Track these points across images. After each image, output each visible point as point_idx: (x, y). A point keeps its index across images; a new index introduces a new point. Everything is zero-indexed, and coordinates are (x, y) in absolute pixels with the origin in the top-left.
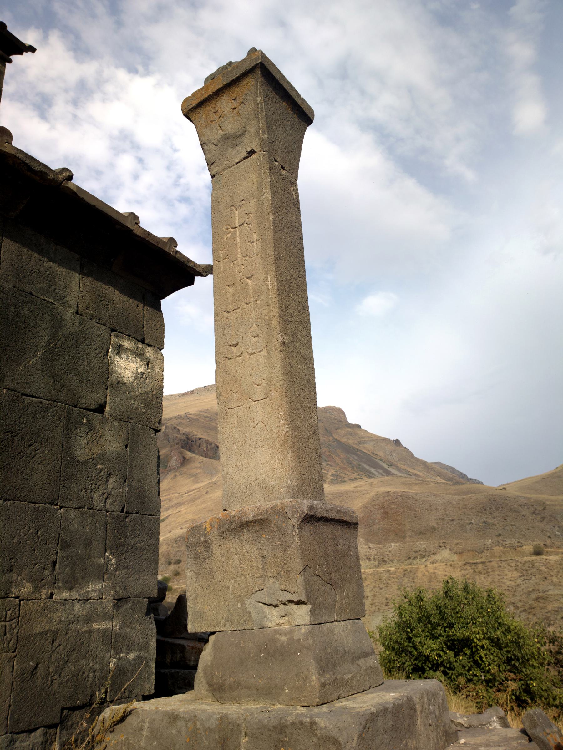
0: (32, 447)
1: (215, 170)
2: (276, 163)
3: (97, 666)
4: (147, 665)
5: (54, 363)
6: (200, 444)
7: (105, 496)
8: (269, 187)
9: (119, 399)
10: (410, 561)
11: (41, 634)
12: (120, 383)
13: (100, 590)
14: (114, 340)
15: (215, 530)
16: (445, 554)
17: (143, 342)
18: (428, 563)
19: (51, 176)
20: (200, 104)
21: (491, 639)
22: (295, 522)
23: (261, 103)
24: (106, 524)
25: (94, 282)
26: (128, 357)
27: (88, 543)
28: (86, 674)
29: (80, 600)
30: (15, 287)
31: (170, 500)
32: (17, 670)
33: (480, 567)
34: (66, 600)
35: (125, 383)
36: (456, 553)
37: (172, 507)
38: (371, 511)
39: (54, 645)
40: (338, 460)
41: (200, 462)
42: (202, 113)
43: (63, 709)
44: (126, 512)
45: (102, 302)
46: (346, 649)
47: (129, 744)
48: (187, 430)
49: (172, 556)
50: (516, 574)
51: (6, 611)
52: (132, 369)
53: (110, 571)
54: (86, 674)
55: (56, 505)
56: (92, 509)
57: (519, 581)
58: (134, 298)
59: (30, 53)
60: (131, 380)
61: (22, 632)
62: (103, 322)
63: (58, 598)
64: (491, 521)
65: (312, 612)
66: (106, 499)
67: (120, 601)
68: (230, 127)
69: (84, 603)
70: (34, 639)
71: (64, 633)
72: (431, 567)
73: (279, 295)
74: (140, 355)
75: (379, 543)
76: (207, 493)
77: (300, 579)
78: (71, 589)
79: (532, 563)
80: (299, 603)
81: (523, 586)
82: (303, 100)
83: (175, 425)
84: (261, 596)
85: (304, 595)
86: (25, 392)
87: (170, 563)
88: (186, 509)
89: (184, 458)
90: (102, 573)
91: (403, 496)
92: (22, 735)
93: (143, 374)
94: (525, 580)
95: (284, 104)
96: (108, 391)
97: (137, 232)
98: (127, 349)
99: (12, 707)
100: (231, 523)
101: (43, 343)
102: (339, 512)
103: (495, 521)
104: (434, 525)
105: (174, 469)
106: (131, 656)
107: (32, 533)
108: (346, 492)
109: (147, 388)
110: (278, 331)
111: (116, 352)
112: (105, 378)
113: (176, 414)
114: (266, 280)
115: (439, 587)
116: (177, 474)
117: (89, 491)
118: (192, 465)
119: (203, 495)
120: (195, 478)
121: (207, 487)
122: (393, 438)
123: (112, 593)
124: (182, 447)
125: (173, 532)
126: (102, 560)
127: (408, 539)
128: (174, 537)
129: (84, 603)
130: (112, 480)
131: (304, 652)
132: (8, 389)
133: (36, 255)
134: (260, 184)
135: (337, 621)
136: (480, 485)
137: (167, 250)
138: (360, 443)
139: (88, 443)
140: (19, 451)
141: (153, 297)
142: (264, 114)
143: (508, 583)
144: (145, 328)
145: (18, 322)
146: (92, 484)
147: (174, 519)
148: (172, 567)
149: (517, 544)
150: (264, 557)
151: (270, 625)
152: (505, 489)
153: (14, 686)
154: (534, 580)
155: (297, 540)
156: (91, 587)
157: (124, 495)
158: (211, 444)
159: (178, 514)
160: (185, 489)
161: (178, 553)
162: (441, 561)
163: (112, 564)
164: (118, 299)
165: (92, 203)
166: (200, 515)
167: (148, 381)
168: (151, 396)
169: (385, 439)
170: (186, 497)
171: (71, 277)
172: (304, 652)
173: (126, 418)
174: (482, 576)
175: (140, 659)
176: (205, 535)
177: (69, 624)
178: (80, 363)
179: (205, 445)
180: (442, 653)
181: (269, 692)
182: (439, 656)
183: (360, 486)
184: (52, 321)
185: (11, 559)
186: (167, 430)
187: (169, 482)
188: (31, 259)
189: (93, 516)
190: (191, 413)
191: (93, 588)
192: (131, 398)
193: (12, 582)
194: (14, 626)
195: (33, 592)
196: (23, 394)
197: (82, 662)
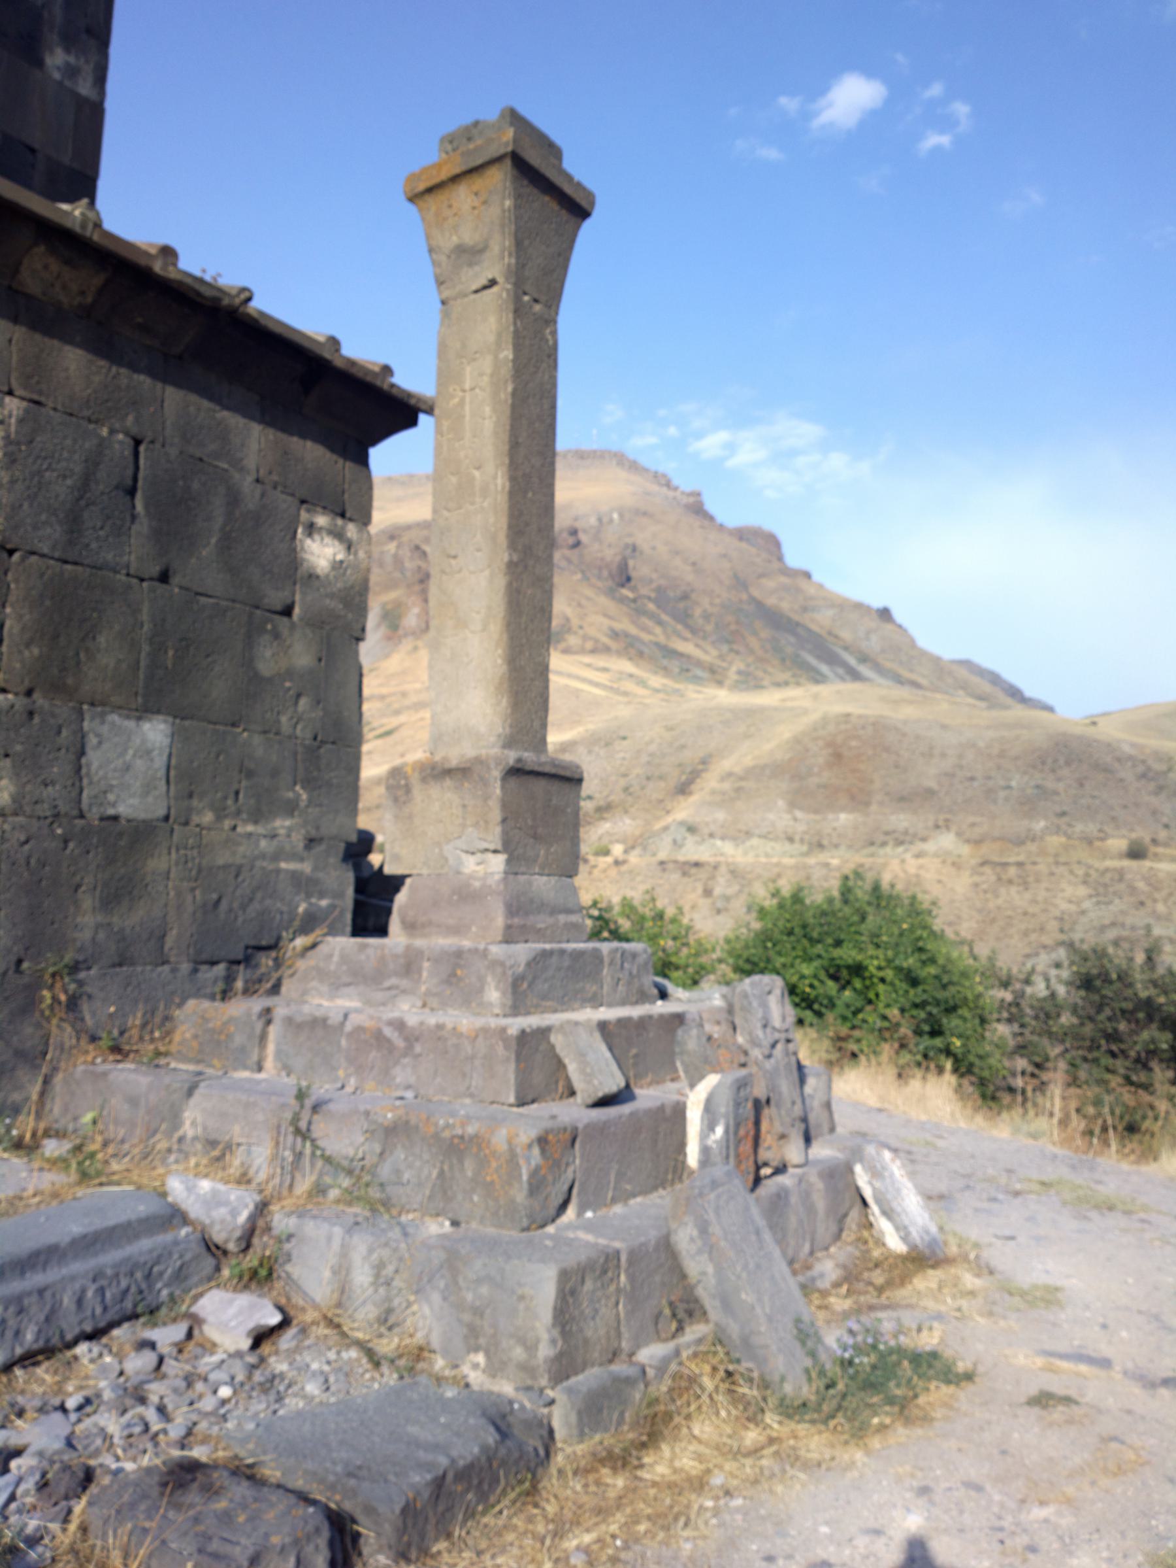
1: (446, 294)
3: (285, 909)
4: (342, 913)
10: (872, 849)
12: (312, 577)
14: (304, 515)
15: (416, 775)
16: (947, 841)
18: (908, 856)
19: (226, 302)
20: (430, 190)
21: (899, 969)
22: (497, 773)
24: (295, 754)
25: (280, 435)
27: (275, 773)
33: (1012, 871)
36: (968, 841)
37: (408, 708)
38: (807, 750)
40: (753, 642)
42: (432, 202)
43: (247, 947)
50: (1082, 891)
57: (1087, 905)
64: (1050, 784)
65: (509, 862)
67: (311, 842)
68: (468, 235)
72: (912, 865)
74: (339, 535)
75: (816, 812)
78: (256, 822)
79: (1121, 875)
80: (495, 851)
81: (1092, 915)
82: (579, 185)
84: (461, 844)
86: (200, 590)
90: (291, 808)
91: (879, 726)
93: (341, 562)
94: (1098, 903)
95: (547, 198)
97: (338, 363)
102: (555, 766)
103: (1061, 786)
104: (932, 784)
105: (413, 633)
106: (324, 903)
108: (762, 710)
112: (292, 568)
114: (495, 477)
115: (834, 886)
116: (420, 643)
122: (877, 603)
127: (874, 807)
132: (181, 588)
134: (499, 335)
136: (1044, 715)
138: (805, 609)
141: (357, 453)
143: (1064, 906)
149: (1095, 834)
152: (1094, 723)
154: (1117, 905)
156: (278, 823)
162: (936, 855)
164: (312, 454)
165: (278, 330)
169: (859, 606)
173: (318, 622)
174: (1013, 890)
175: (332, 907)
176: (406, 778)
180: (816, 983)
181: (457, 930)
182: (811, 986)
183: (793, 699)
191: (281, 824)
192: (327, 596)
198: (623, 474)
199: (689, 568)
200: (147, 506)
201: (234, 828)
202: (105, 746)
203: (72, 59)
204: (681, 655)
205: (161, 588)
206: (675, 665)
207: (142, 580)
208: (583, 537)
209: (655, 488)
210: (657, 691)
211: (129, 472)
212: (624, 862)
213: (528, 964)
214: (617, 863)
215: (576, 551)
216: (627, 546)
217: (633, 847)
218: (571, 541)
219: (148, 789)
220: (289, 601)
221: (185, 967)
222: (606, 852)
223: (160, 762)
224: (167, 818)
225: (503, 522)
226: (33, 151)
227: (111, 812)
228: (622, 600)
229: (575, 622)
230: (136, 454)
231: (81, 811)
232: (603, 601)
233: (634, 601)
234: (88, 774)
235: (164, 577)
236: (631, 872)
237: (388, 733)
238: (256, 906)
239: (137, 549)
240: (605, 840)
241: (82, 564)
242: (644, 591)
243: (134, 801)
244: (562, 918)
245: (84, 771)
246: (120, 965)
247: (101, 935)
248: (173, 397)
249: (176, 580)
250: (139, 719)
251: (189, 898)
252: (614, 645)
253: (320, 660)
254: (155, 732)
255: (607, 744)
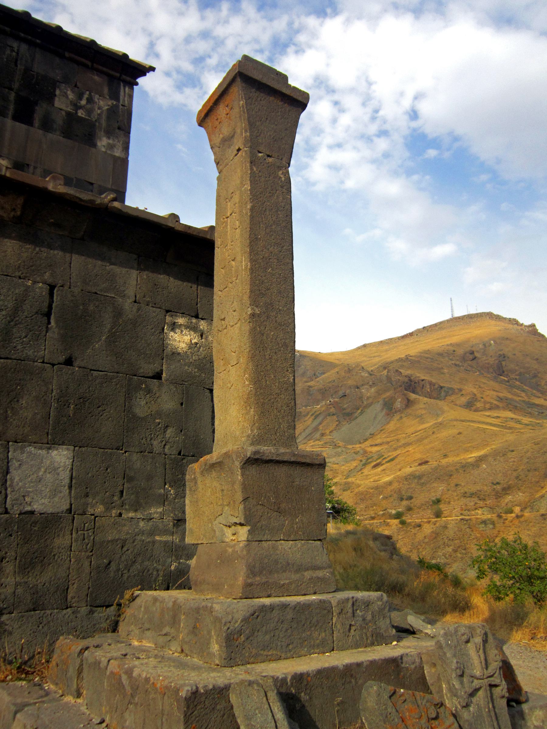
0: (100, 409)
2: (260, 155)
5: (117, 343)
6: (423, 386)
7: (164, 443)
8: (248, 179)
9: (174, 366)
11: (112, 541)
12: (175, 354)
13: (161, 513)
14: (168, 319)
17: (197, 317)
22: (237, 464)
23: (243, 106)
24: (165, 464)
25: (150, 274)
26: (182, 331)
27: (150, 478)
28: (150, 572)
29: (144, 519)
30: (82, 290)
31: (398, 440)
32: (94, 564)
34: (132, 518)
35: (180, 353)
37: (400, 447)
39: (124, 549)
41: (425, 404)
44: (183, 455)
45: (158, 290)
46: (289, 561)
47: (135, 616)
48: (409, 372)
49: (403, 493)
51: (84, 524)
52: (186, 341)
53: (170, 499)
54: (150, 572)
55: (122, 450)
56: (152, 453)
58: (188, 281)
59: (151, 73)
60: (185, 350)
61: (97, 539)
62: (159, 306)
63: (126, 517)
66: (165, 445)
69: (148, 521)
70: (107, 544)
71: (131, 541)
73: (251, 273)
74: (194, 329)
76: (433, 433)
77: (241, 507)
78: (136, 511)
80: (241, 525)
83: (397, 368)
84: (221, 519)
85: (243, 519)
87: (402, 499)
88: (414, 449)
89: (408, 400)
92: (99, 608)
93: (196, 344)
95: (272, 98)
96: (164, 361)
97: (178, 228)
98: (181, 325)
99: (91, 589)
100: (206, 465)
101: (106, 330)
105: (399, 411)
107: (103, 470)
109: (201, 355)
110: (248, 306)
111: (170, 329)
112: (162, 350)
113: (397, 358)
116: (403, 415)
117: (149, 439)
118: (417, 406)
119: (430, 435)
120: (421, 419)
121: (433, 427)
123: (172, 515)
124: (406, 390)
125: (403, 470)
126: (162, 491)
128: (404, 475)
129: (148, 521)
130: (169, 431)
131: (239, 560)
133: (100, 263)
135: (284, 540)
137: (208, 237)
139: (147, 403)
140: (89, 412)
142: (246, 115)
144: (199, 305)
145: (85, 316)
146: (151, 434)
147: (403, 458)
148: (405, 503)
150: (223, 490)
151: (227, 540)
153: (92, 575)
155: (239, 478)
156: (153, 510)
157: (180, 442)
158: (434, 385)
159: (407, 453)
160: (412, 430)
161: (409, 490)
163: (171, 494)
164: (172, 285)
166: (428, 454)
167: (201, 349)
168: (204, 361)
170: (413, 438)
171: (129, 274)
172: (239, 560)
173: (178, 382)
177: (136, 536)
178: (138, 342)
179: (428, 387)
184: (114, 311)
185: (87, 488)
186: (389, 374)
187: (396, 424)
188: (96, 266)
189: (153, 458)
190: (411, 355)
191: (155, 511)
193: (88, 504)
194: (90, 534)
195: (105, 512)
196: (91, 370)
197: (146, 563)
198: (493, 322)
199: (535, 362)
200: (57, 322)
201: (120, 515)
202: (24, 467)
203: (111, 141)
204: (538, 405)
205: (65, 368)
206: (535, 411)
207: (53, 365)
208: (476, 354)
209: (510, 326)
210: (526, 425)
211: (46, 304)
212: (522, 516)
213: (246, 620)
214: (517, 517)
215: (475, 361)
216: (500, 356)
217: (525, 508)
218: (471, 357)
219: (54, 492)
220: (158, 370)
221: (84, 610)
222: (511, 512)
223: (65, 476)
224: (70, 511)
225: (247, 288)
226: (92, 184)
227: (28, 508)
228: (502, 382)
229: (479, 395)
230: (51, 294)
231: (6, 509)
232: (492, 383)
233: (508, 382)
234: (11, 486)
235: (69, 362)
236: (526, 521)
237: (392, 460)
238: (137, 566)
239: (50, 346)
240: (510, 505)
241: (11, 359)
242: (513, 376)
243: (46, 501)
244: (308, 574)
245: (8, 483)
246: (34, 610)
247: (20, 590)
248: (77, 261)
249: (76, 363)
250: (49, 448)
251: (87, 564)
252: (501, 405)
253: (182, 404)
254: (61, 457)
255: (504, 455)
